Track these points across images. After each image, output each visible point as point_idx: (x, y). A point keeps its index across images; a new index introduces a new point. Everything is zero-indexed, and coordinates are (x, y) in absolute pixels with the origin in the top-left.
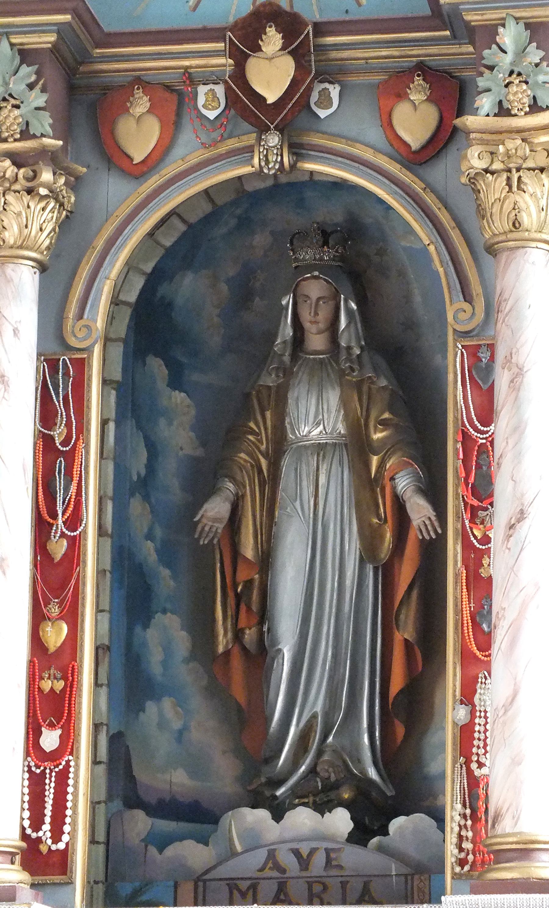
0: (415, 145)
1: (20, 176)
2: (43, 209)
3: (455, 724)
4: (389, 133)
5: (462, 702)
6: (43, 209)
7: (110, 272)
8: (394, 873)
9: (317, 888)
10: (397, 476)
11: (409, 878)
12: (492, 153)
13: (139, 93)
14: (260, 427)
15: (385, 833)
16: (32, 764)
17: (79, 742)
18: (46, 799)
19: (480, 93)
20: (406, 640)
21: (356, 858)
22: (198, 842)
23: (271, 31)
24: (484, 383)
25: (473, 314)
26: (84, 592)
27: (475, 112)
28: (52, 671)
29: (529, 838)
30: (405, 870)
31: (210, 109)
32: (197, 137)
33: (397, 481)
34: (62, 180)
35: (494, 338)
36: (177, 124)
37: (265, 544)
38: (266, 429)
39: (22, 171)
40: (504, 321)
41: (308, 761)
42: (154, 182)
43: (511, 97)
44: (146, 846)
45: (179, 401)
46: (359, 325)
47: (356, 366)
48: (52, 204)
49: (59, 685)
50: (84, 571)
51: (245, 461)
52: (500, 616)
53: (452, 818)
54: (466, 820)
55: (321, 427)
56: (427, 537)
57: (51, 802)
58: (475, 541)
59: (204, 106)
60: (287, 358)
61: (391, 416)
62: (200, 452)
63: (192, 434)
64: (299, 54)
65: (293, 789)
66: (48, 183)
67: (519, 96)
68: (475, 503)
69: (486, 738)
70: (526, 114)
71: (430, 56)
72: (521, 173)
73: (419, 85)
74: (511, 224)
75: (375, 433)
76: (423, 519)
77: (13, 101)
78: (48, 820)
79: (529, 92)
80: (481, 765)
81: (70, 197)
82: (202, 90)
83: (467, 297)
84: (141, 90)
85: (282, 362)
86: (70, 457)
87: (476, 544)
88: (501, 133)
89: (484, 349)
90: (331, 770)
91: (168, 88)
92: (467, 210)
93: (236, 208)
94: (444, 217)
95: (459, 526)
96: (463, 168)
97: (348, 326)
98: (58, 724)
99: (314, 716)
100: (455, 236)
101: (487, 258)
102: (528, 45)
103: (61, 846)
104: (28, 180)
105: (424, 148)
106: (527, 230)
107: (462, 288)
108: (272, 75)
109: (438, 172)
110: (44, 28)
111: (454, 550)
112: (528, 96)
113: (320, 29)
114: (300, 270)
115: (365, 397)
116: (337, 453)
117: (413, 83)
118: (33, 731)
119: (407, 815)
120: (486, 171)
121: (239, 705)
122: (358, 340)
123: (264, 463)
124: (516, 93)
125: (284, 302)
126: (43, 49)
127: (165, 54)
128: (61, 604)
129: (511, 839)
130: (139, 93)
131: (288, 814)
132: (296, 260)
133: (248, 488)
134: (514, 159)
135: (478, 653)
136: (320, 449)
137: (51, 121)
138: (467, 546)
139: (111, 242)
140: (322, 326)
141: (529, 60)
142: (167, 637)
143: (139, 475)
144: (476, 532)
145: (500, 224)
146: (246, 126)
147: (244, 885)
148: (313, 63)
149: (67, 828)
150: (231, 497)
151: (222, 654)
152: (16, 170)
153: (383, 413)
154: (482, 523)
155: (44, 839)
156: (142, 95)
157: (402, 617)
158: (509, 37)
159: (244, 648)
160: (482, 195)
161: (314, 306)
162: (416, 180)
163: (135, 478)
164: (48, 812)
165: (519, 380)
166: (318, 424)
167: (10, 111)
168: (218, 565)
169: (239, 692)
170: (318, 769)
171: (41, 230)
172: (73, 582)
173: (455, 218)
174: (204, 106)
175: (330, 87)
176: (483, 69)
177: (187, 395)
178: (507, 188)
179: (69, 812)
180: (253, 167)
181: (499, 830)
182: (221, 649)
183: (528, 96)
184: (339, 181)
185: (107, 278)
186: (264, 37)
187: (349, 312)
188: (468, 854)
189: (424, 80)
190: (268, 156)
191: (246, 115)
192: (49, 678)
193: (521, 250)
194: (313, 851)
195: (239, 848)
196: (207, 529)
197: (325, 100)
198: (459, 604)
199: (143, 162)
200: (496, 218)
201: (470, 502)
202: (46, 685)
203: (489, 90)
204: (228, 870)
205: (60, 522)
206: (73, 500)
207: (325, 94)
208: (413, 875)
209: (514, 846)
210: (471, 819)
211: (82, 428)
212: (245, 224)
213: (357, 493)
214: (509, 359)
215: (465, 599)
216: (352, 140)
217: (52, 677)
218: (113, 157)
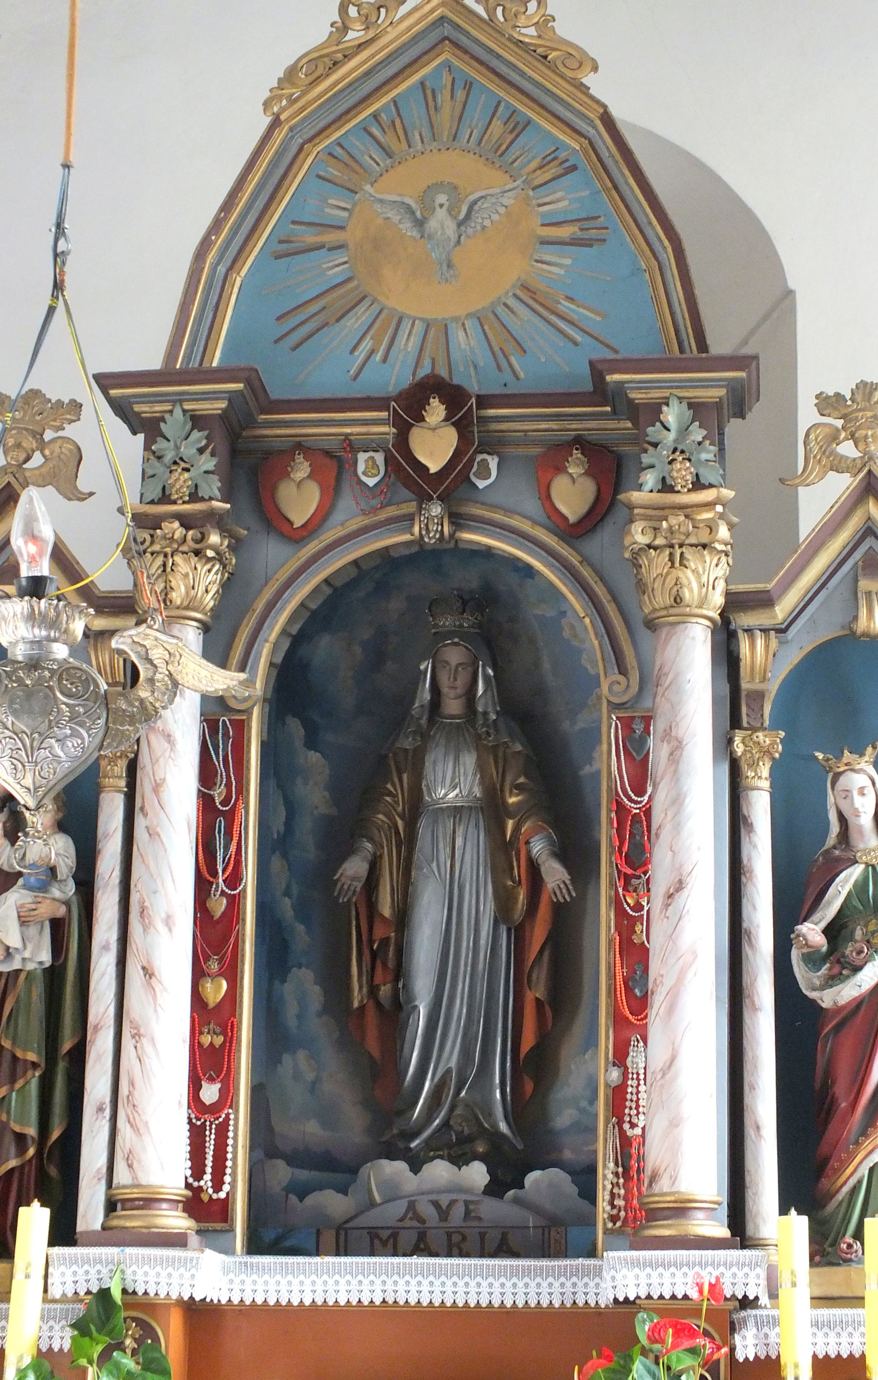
0: (572, 519)
1: (189, 537)
2: (209, 571)
3: (607, 1085)
4: (547, 505)
5: (614, 1065)
6: (209, 571)
7: (270, 635)
8: (531, 1225)
9: (456, 1238)
10: (532, 840)
11: (546, 1230)
12: (655, 529)
13: (299, 458)
14: (397, 789)
15: (522, 1187)
16: (193, 1116)
17: (238, 1096)
18: (207, 1150)
19: (644, 469)
20: (537, 999)
21: (494, 1210)
22: (338, 1192)
23: (435, 402)
24: (638, 754)
25: (628, 686)
26: (243, 950)
27: (639, 487)
28: (211, 1026)
29: (687, 1197)
30: (544, 1223)
31: (369, 476)
32: (357, 503)
33: (532, 845)
34: (226, 543)
35: (652, 710)
37: (401, 905)
38: (402, 790)
39: (191, 533)
40: (663, 695)
41: (442, 1114)
42: (312, 547)
43: (675, 474)
44: (287, 1196)
45: (314, 760)
46: (495, 690)
47: (491, 731)
48: (217, 567)
49: (219, 1040)
50: (244, 929)
51: (383, 821)
52: (658, 982)
53: (604, 1176)
54: (619, 1178)
55: (457, 791)
56: (562, 900)
57: (211, 1153)
58: (628, 908)
59: (364, 473)
60: (424, 721)
61: (526, 781)
62: (334, 811)
63: (326, 794)
64: (462, 426)
65: (427, 1142)
66: (215, 545)
68: (629, 871)
69: (638, 1099)
70: (689, 490)
71: (589, 430)
72: (684, 549)
73: (577, 458)
74: (672, 600)
75: (510, 796)
76: (558, 882)
77: (183, 465)
78: (209, 1170)
79: (692, 470)
80: (633, 1126)
81: (231, 559)
82: (362, 457)
83: (623, 670)
84: (302, 456)
85: (420, 725)
86: (230, 817)
87: (629, 911)
88: (663, 509)
89: (637, 720)
90: (464, 1124)
91: (328, 454)
92: (625, 584)
93: (382, 572)
94: (600, 590)
95: (613, 893)
96: (627, 543)
97: (485, 692)
98: (218, 1077)
99: (449, 1071)
100: (611, 610)
101: (643, 633)
102: (691, 423)
103: (222, 1195)
104: (197, 542)
106: (688, 606)
107: (617, 660)
108: (434, 445)
109: (595, 545)
110: (220, 395)
111: (606, 916)
112: (691, 473)
113: (484, 401)
114: (441, 636)
115: (501, 764)
116: (473, 815)
117: (572, 456)
118: (195, 1085)
119: (543, 1169)
120: (649, 546)
121: (371, 1057)
122: (494, 705)
123: (400, 823)
124: (680, 470)
125: (422, 667)
126: (213, 415)
127: (328, 421)
128: (220, 961)
129: (668, 1199)
130: (299, 458)
131: (425, 1166)
132: (436, 626)
133: (386, 848)
134: (677, 535)
135: (631, 1017)
136: (456, 811)
137: (219, 484)
138: (620, 912)
140: (460, 691)
141: (692, 438)
142: (304, 986)
143: (278, 833)
144: (629, 901)
145: (662, 599)
146: (405, 493)
147: (385, 1234)
148: (476, 435)
149: (227, 1179)
150: (370, 857)
151: (357, 1009)
152: (184, 532)
153: (519, 777)
154: (635, 890)
155: (205, 1188)
156: (302, 460)
157: (534, 976)
158: (672, 415)
159: (379, 1005)
160: (643, 570)
161: (451, 673)
162: (574, 553)
163: (275, 836)
164: (209, 1162)
165: (678, 752)
166: (455, 788)
167: (180, 474)
168: (354, 923)
169: (373, 1046)
170: (452, 1123)
171: (207, 591)
172: (232, 940)
173: (610, 591)
174: (364, 473)
175: (489, 458)
176: (646, 446)
177: (322, 754)
178: (670, 564)
179: (229, 1163)
180: (412, 535)
181: (656, 1189)
182: (356, 1004)
183: (691, 473)
184: (483, 548)
185: (266, 641)
186: (427, 408)
187: (486, 678)
188: (620, 1211)
189: (582, 453)
190: (431, 522)
191: (408, 482)
192: (208, 1033)
193: (681, 626)
194: (452, 1203)
195: (378, 1198)
196: (346, 887)
197: (484, 473)
198: (612, 969)
199: (303, 526)
200: (658, 593)
201: (623, 870)
202: (206, 1040)
203: (652, 467)
204: (370, 1219)
205: (221, 880)
206: (232, 859)
207: (484, 464)
208: (549, 1227)
209: (671, 1205)
210: (623, 1177)
211: (242, 790)
212: (382, 589)
213: (493, 856)
214: (668, 735)
215: (618, 964)
216: (508, 511)
217: (212, 1032)
218: (273, 520)
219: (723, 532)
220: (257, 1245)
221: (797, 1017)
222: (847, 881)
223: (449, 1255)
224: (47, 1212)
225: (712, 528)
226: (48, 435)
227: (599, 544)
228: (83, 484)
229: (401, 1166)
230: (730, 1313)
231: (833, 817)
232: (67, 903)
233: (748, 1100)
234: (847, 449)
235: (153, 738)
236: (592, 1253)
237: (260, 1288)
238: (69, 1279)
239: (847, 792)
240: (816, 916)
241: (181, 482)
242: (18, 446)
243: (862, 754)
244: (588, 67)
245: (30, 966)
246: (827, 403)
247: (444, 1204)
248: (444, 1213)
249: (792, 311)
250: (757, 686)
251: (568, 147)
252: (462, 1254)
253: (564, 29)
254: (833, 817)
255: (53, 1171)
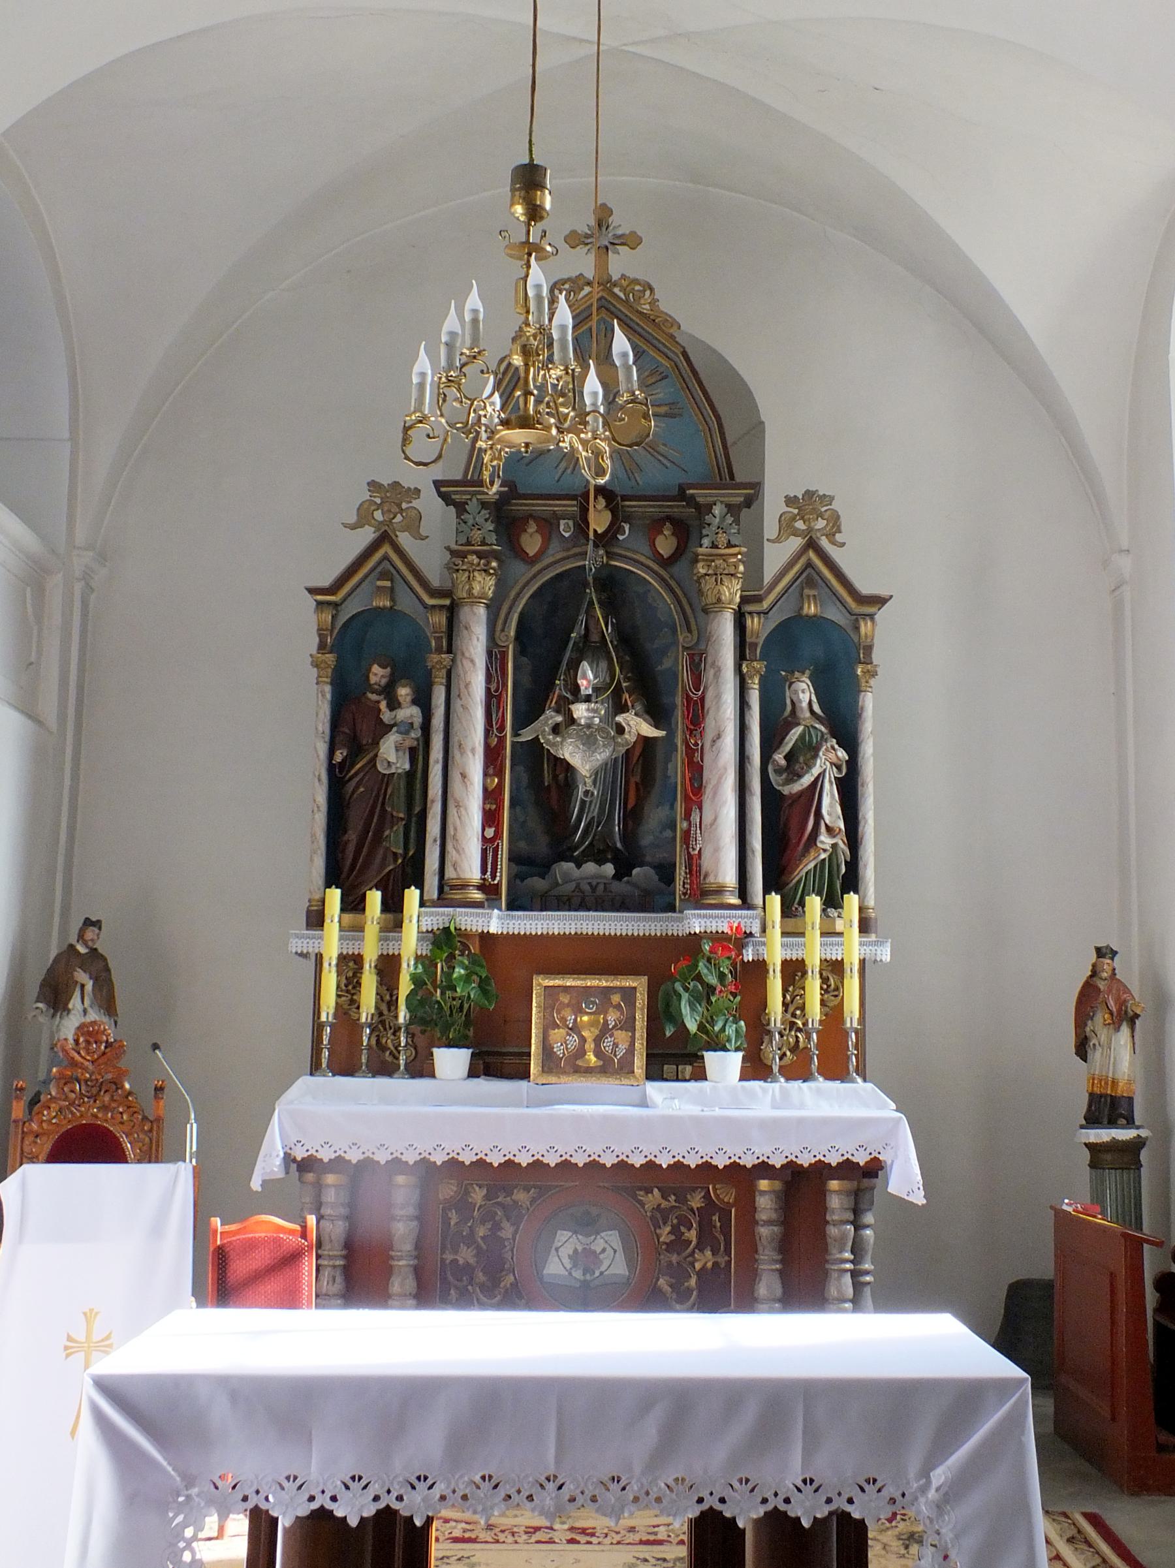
13: (531, 522)
21: (620, 887)
27: (701, 546)
36: (549, 539)
42: (538, 567)
49: (494, 807)
64: (614, 512)
67: (722, 539)
82: (562, 522)
83: (690, 631)
86: (499, 698)
91: (545, 520)
101: (700, 614)
105: (669, 558)
108: (599, 521)
109: (676, 569)
113: (625, 498)
130: (531, 522)
139: (518, 594)
158: (717, 510)
164: (489, 867)
202: (487, 807)
204: (554, 892)
211: (505, 685)
214: (713, 663)
218: (519, 553)
219: (741, 568)
220: (512, 906)
221: (770, 796)
222: (796, 732)
223: (596, 910)
224: (338, 891)
225: (736, 567)
226: (404, 506)
227: (679, 568)
228: (423, 531)
229: (572, 865)
230: (742, 939)
231: (788, 702)
232: (417, 739)
233: (748, 837)
234: (800, 525)
235: (465, 662)
236: (672, 908)
237: (517, 926)
238: (429, 923)
239: (796, 692)
240: (780, 751)
241: (477, 535)
242: (389, 511)
243: (803, 673)
244: (675, 328)
245: (400, 771)
246: (790, 501)
247: (594, 883)
248: (594, 889)
249: (763, 431)
250: (753, 640)
251: (662, 365)
252: (604, 910)
253: (663, 306)
254: (788, 702)
255: (409, 870)
